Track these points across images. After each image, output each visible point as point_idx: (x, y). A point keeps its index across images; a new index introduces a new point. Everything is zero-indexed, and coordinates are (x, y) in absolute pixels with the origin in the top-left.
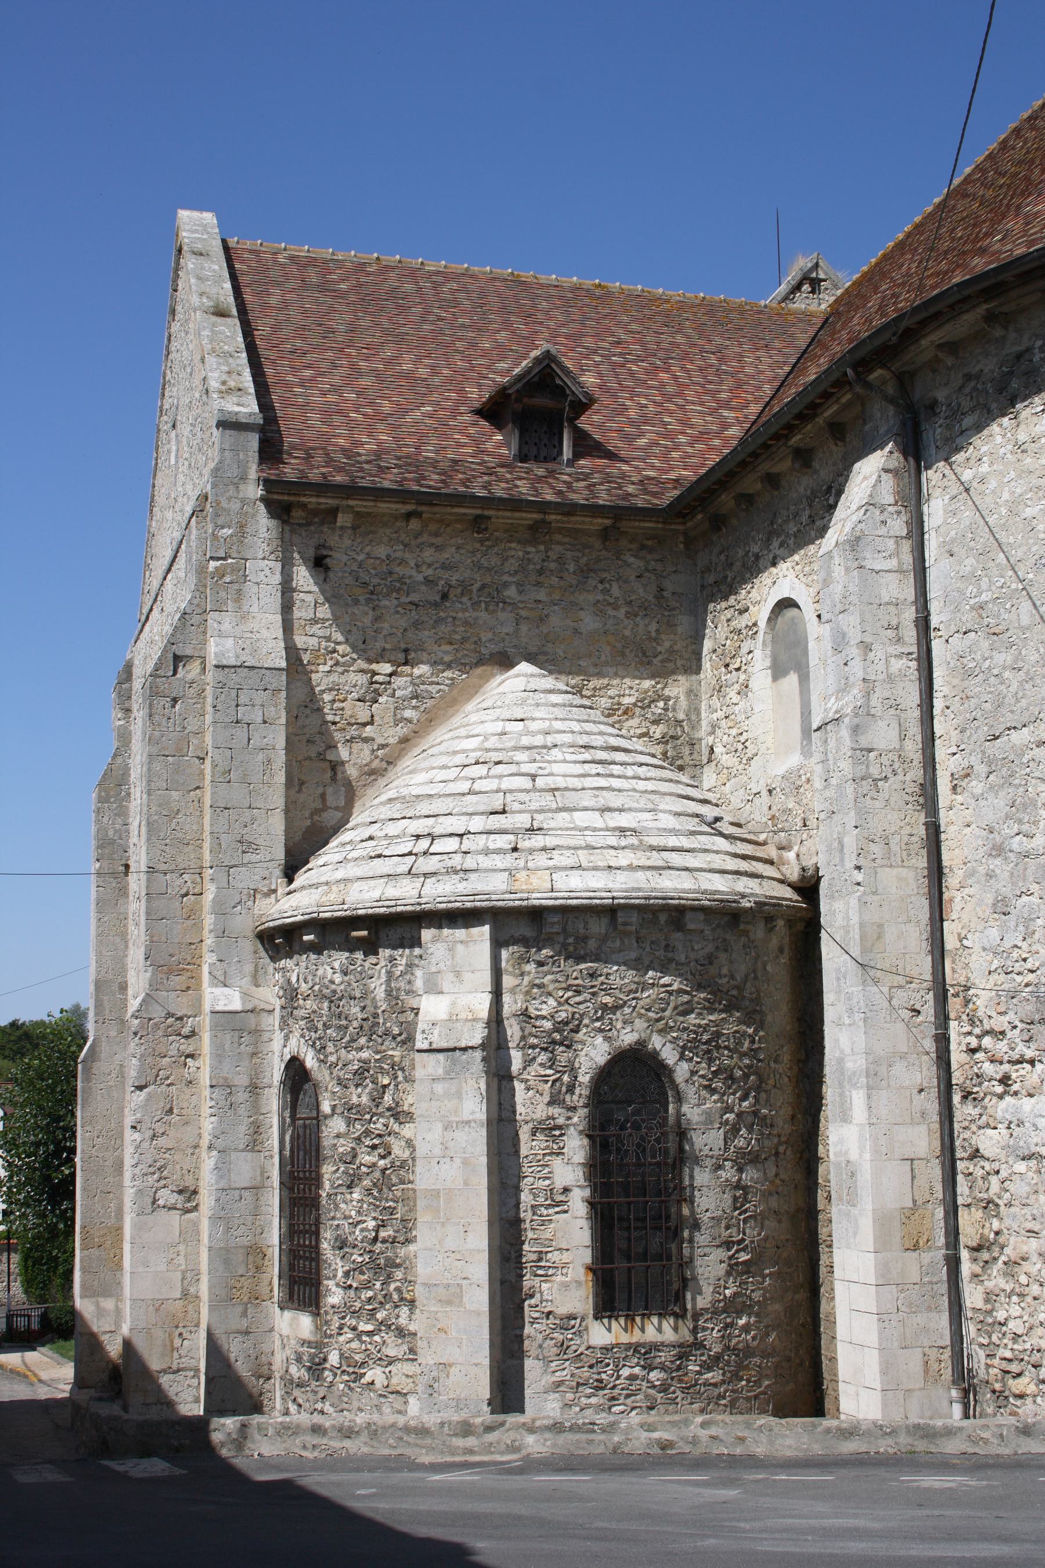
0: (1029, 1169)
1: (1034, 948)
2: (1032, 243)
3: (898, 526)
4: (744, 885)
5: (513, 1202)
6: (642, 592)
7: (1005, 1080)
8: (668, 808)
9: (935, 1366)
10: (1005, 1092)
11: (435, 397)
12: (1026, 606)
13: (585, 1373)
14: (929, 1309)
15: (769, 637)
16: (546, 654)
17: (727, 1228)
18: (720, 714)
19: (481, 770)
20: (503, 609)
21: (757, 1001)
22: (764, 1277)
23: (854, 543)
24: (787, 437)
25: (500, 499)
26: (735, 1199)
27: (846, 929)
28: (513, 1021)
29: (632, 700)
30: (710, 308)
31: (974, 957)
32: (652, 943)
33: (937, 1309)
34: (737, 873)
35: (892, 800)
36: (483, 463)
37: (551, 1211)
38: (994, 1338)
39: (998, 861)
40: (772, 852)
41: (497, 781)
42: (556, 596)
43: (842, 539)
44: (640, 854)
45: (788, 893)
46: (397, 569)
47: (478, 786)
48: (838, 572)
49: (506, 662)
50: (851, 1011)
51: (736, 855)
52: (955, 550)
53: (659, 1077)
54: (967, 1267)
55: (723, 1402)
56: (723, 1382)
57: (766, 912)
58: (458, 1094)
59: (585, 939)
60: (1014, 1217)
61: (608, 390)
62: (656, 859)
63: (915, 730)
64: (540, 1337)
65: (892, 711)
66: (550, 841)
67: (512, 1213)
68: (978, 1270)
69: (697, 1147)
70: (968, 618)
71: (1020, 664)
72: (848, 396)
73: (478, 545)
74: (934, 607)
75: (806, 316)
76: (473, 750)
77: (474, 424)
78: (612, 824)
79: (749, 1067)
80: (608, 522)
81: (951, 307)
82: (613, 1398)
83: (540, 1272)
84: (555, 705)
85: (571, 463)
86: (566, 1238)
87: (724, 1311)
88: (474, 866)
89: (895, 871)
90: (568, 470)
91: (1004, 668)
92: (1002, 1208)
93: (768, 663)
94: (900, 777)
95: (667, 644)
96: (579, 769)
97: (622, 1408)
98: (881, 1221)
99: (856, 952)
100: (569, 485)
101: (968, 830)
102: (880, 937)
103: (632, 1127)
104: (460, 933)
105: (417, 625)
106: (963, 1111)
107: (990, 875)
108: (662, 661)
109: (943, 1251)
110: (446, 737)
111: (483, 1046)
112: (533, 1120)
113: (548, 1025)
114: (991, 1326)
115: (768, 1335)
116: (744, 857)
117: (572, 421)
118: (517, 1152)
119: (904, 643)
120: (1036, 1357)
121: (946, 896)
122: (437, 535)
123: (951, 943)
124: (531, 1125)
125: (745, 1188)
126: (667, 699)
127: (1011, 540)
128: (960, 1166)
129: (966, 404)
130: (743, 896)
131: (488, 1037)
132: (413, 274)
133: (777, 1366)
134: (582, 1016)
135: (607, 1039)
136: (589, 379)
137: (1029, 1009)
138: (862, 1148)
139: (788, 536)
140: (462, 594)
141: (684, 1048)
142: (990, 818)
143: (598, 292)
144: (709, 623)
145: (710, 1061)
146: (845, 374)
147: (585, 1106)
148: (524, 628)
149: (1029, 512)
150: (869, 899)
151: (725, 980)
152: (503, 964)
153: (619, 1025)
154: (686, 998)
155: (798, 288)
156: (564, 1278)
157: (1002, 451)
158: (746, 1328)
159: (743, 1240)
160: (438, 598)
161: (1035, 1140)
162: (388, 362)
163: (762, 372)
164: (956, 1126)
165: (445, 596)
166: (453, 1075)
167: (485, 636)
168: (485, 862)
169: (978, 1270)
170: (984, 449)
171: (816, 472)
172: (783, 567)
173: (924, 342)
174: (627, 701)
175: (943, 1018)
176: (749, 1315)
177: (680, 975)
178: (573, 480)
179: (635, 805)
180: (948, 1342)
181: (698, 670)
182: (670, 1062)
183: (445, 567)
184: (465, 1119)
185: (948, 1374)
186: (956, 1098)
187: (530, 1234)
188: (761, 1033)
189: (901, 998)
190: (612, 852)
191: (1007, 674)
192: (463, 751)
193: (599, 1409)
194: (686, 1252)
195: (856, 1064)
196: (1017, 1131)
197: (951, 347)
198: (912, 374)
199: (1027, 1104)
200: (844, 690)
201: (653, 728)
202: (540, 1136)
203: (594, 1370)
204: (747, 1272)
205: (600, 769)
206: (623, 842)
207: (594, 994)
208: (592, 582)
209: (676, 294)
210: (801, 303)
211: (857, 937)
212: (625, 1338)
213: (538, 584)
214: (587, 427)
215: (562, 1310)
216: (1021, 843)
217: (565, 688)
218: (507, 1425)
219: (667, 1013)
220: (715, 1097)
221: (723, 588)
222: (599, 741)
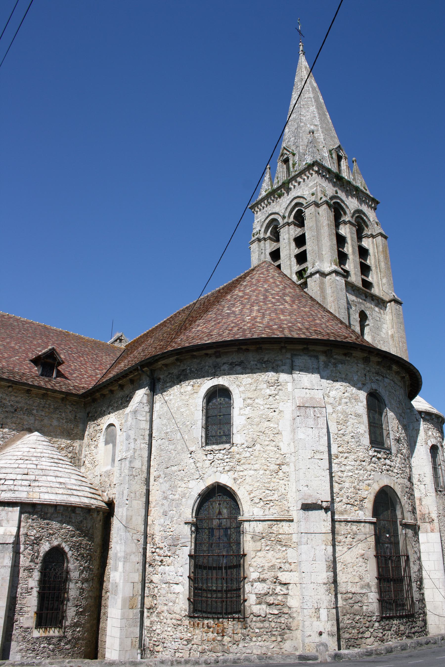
0: (166, 586)
1: (173, 525)
2: (189, 343)
3: (147, 409)
4: (93, 501)
5: (15, 591)
6: (71, 416)
7: (162, 561)
8: (73, 478)
9: (134, 643)
10: (161, 565)
11: (20, 355)
12: (179, 434)
13: (30, 646)
14: (134, 626)
15: (105, 433)
16: (42, 430)
17: (77, 601)
18: (88, 452)
19: (21, 461)
20: (32, 416)
21: (92, 535)
22: (86, 616)
23: (135, 412)
24: (118, 381)
25: (36, 386)
26: (80, 592)
27: (122, 516)
28: (23, 536)
29: (64, 446)
30: (95, 343)
31: (156, 527)
32: (66, 516)
33: (136, 626)
34: (91, 498)
35: (138, 482)
36: (31, 375)
37: (26, 595)
38: (152, 635)
39: (165, 501)
40: (100, 493)
41: (26, 465)
42: (47, 414)
43: (132, 410)
44: (65, 490)
45: (104, 505)
46: (3, 401)
47: (20, 466)
48: (130, 419)
49: (30, 431)
50: (121, 539)
51: (91, 493)
52: (161, 417)
53: (63, 555)
54: (146, 614)
55: (70, 655)
56: (71, 648)
57: (98, 509)
58: (3, 558)
59: (47, 513)
60: (161, 600)
61: (67, 360)
62: (70, 492)
63: (146, 464)
64: (18, 634)
65: (140, 458)
66: (40, 484)
67: (14, 595)
68: (149, 615)
69: (71, 576)
70: (163, 435)
71: (176, 449)
72: (137, 373)
73: (27, 397)
74: (154, 431)
75: (119, 349)
76: (20, 455)
77: (30, 364)
78: (58, 481)
79: (88, 553)
80: (64, 396)
81: (168, 355)
82: (37, 654)
83: (20, 614)
84: (44, 445)
85: (55, 378)
86: (30, 603)
87: (73, 626)
88: (17, 489)
89: (137, 501)
90: (54, 380)
91: (172, 450)
92: (158, 597)
93: (104, 440)
94: (141, 476)
95: (75, 431)
96: (50, 464)
97: (40, 657)
98: (124, 600)
99: (124, 523)
100: (55, 384)
101: (157, 492)
102: (131, 519)
103: (53, 570)
104: (10, 509)
105: (6, 417)
106: (149, 569)
107: (163, 505)
108: (74, 436)
109: (140, 609)
110: (11, 450)
111: (13, 543)
112: (24, 566)
113: (33, 538)
114: (151, 631)
115: (85, 634)
116: (93, 493)
117: (57, 367)
118: (18, 576)
119: (145, 440)
120: (163, 640)
121: (149, 509)
122: (16, 393)
123: (150, 522)
124: (24, 568)
125: (83, 589)
126: (74, 447)
127: (177, 417)
128: (146, 585)
129: (168, 380)
130: (92, 505)
131: (15, 541)
132: (17, 320)
133: (86, 643)
134: (43, 536)
135: (50, 543)
136: (62, 356)
137: (170, 542)
138: (120, 579)
139: (114, 407)
140: (21, 410)
141: (71, 547)
142: (164, 489)
143: (66, 334)
144: (88, 427)
145: (78, 551)
146: (138, 368)
147: (41, 563)
148: (37, 422)
149: (182, 410)
150: (129, 508)
151: (84, 528)
152: (22, 519)
153: (53, 539)
154: (73, 533)
155: (116, 340)
156: (27, 616)
157: (177, 393)
158: (79, 632)
159: (81, 605)
160: (13, 411)
161: (169, 578)
162: (8, 343)
163: (107, 362)
164: (146, 573)
165: (16, 410)
166: (2, 551)
167: (25, 423)
168: (21, 488)
169: (149, 615)
170: (172, 392)
171: (124, 391)
172: (112, 415)
173: (159, 363)
174: (62, 446)
175: (145, 543)
176: (80, 628)
177: (72, 526)
178: (55, 383)
179: (64, 476)
180: (139, 636)
181: (83, 439)
182: (67, 551)
183: (17, 402)
184: (5, 565)
185: (137, 645)
186: (147, 566)
187: (19, 602)
188: (93, 544)
189: (135, 537)
190: (57, 489)
191: (172, 451)
192: (17, 455)
193: (33, 657)
194: (65, 608)
195: (121, 554)
196: (164, 576)
197: (166, 365)
198: (155, 370)
199: (167, 568)
200: (128, 451)
201: (69, 454)
202: (26, 571)
203: (33, 645)
204: (81, 614)
205: (55, 465)
206: (61, 486)
207: (47, 530)
208: (57, 412)
209: (87, 338)
210: (117, 344)
211: (125, 519)
212: (44, 635)
213: (42, 410)
214: (60, 369)
215: (26, 626)
216: (172, 497)
217: (47, 441)
218: (6, 664)
219: (68, 537)
220: (78, 562)
221: (93, 418)
222: (56, 457)
